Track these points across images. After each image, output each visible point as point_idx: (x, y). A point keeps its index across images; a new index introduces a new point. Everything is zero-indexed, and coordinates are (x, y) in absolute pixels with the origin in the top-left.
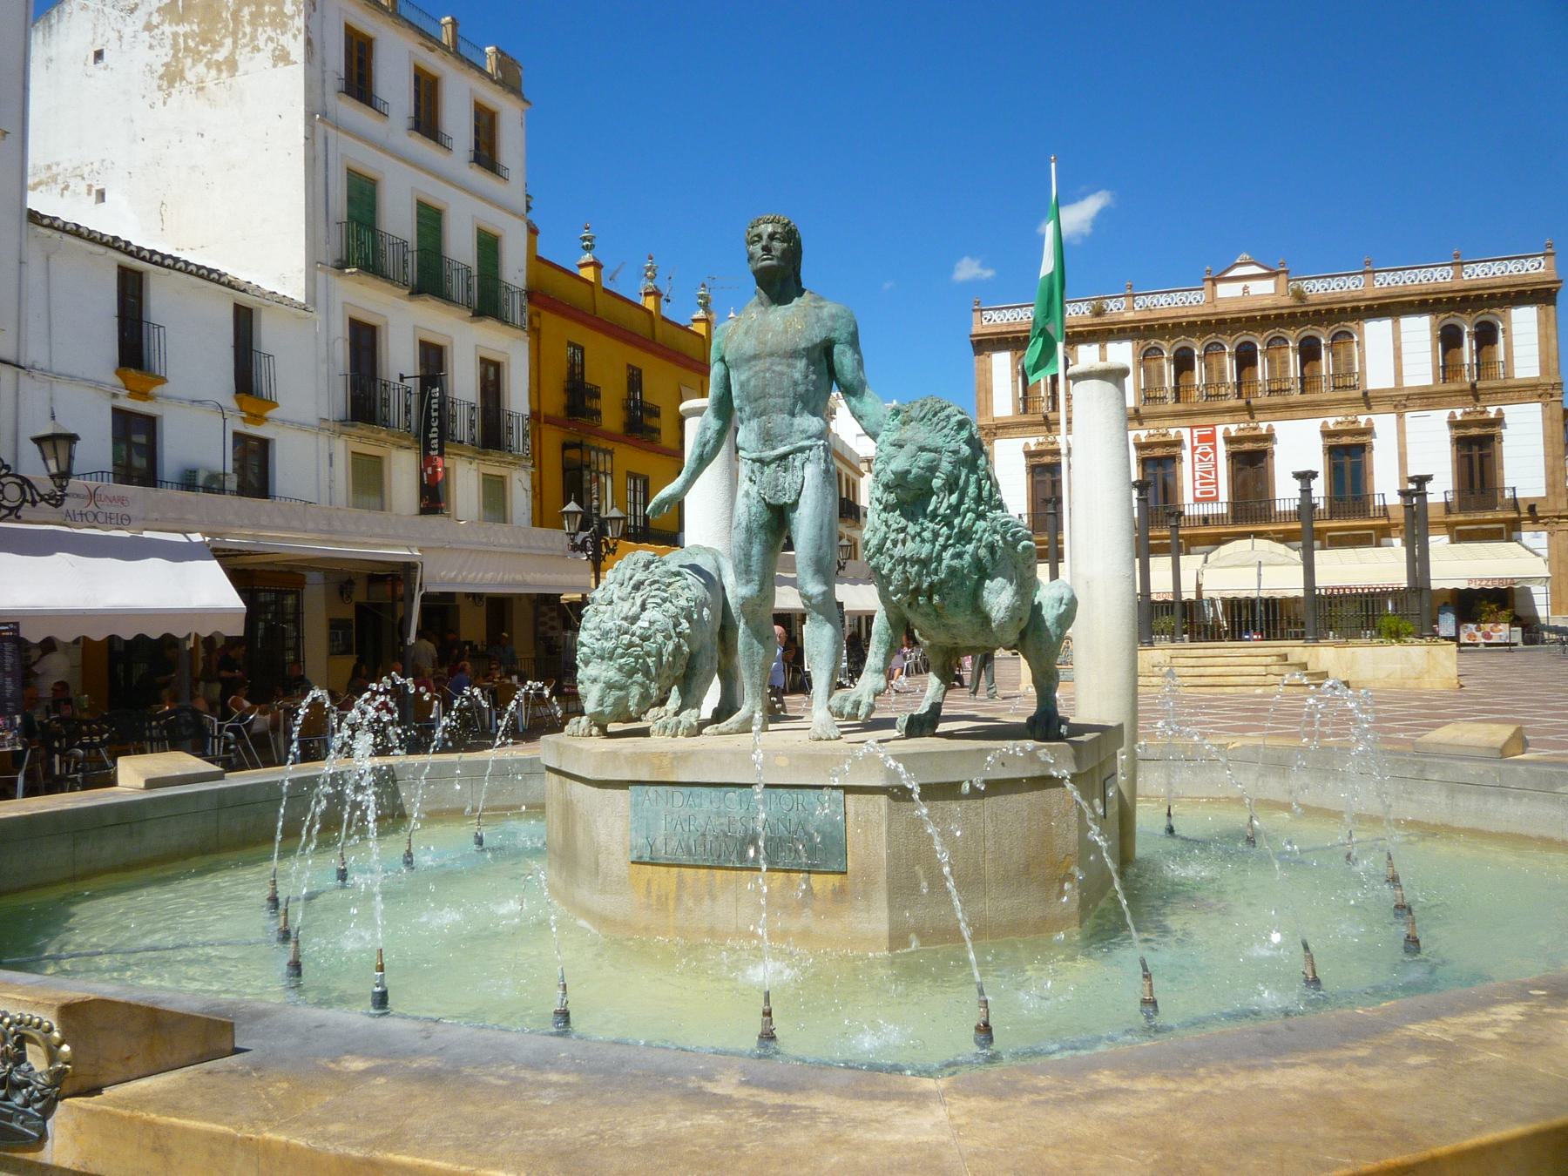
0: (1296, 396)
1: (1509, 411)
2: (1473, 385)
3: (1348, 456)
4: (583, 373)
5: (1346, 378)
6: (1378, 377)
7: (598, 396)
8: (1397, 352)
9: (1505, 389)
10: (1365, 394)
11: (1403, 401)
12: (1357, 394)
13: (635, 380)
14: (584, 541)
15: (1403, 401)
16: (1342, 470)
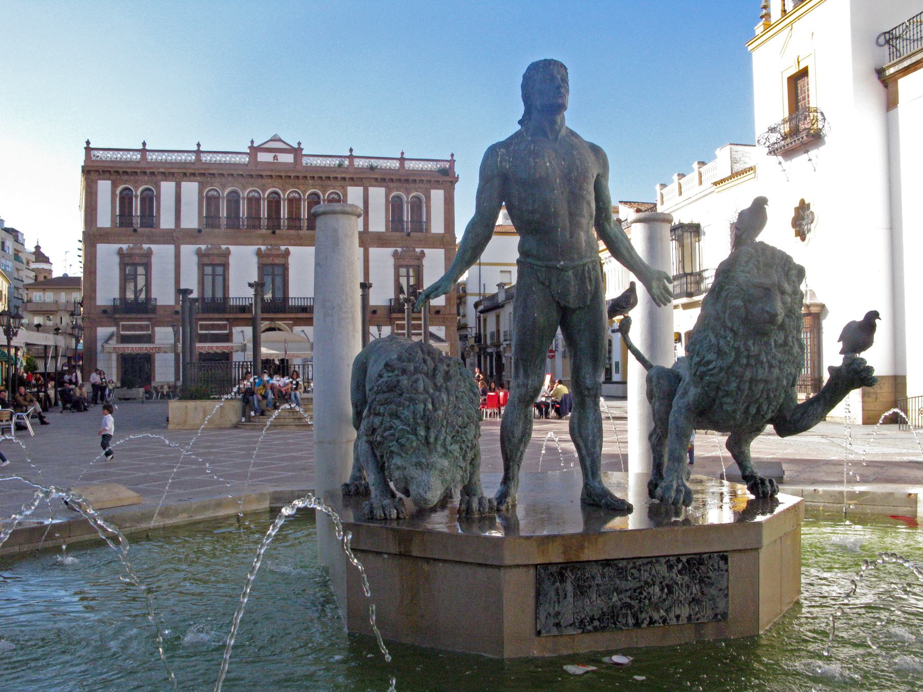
11: (176, 237)
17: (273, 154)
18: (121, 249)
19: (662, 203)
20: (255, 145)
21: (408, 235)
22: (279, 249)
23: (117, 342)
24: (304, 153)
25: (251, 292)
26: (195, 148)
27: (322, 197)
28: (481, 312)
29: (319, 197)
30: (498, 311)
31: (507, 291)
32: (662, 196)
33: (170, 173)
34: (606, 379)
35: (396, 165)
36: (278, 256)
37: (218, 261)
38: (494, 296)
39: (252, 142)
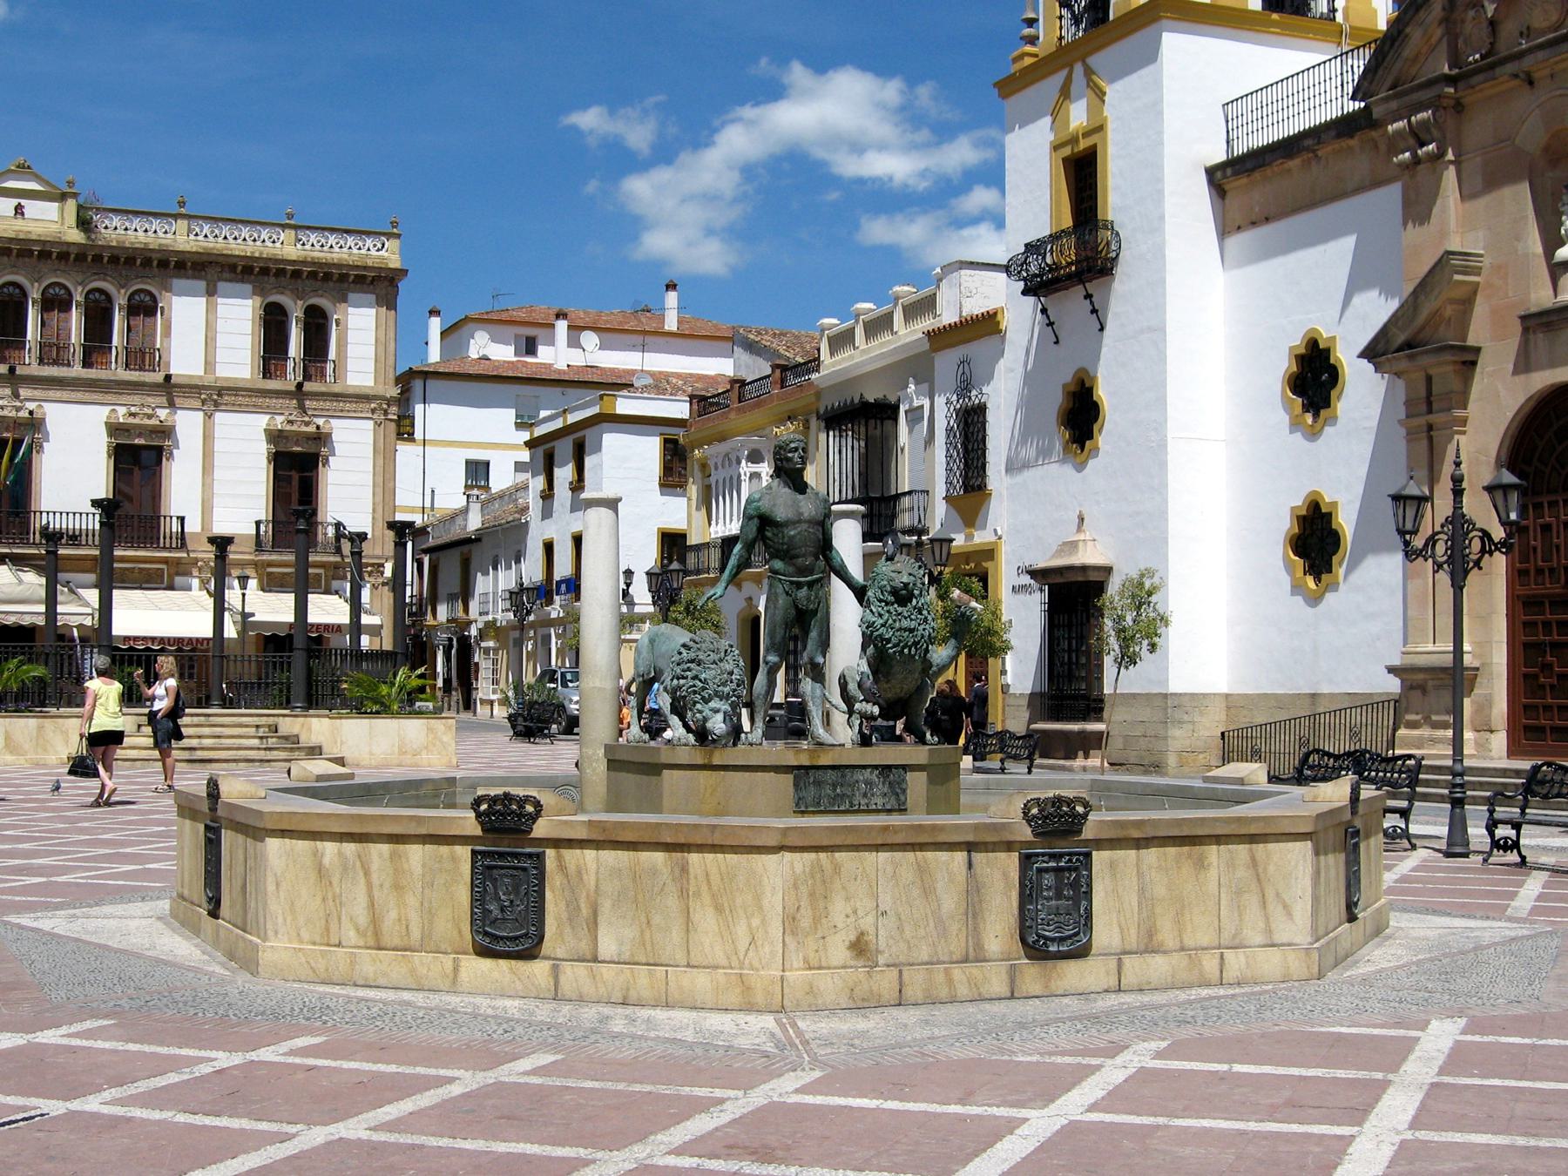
0: (77, 371)
2: (300, 386)
3: (138, 460)
5: (141, 356)
6: (184, 360)
8: (208, 333)
9: (337, 396)
10: (168, 378)
11: (216, 396)
12: (158, 377)
16: (301, 495)
17: (15, 202)
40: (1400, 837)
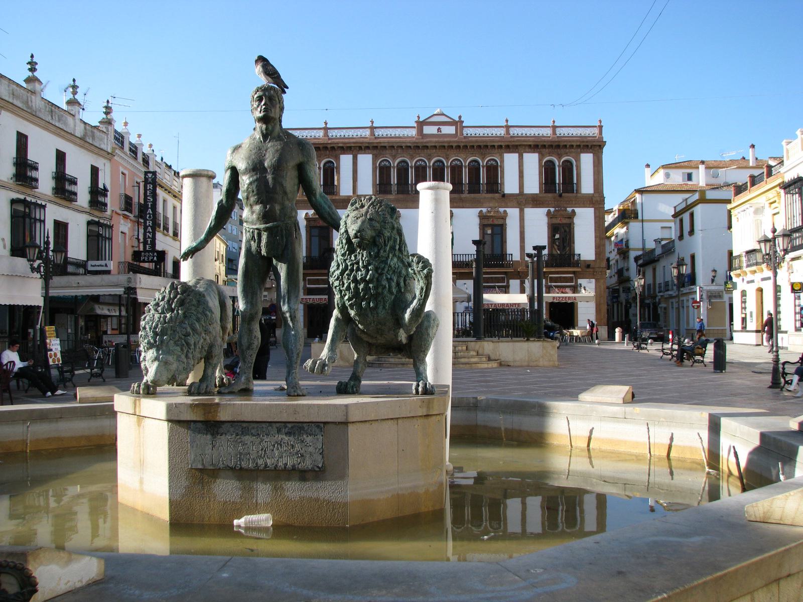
1: (577, 210)
4: (10, 504)
6: (510, 186)
7: (36, 169)
11: (523, 201)
13: (61, 157)
14: (39, 266)
15: (523, 201)
17: (437, 127)
18: (481, 211)
19: (788, 158)
20: (421, 120)
21: (560, 196)
22: (566, 210)
23: (304, 295)
24: (464, 125)
25: (473, 249)
26: (324, 126)
27: (481, 164)
28: (641, 266)
29: (479, 164)
30: (653, 265)
31: (663, 246)
32: (787, 151)
33: (347, 147)
34: (743, 328)
35: (502, 132)
36: (498, 218)
37: (497, 222)
38: (653, 251)
39: (419, 117)
40: (701, 362)
